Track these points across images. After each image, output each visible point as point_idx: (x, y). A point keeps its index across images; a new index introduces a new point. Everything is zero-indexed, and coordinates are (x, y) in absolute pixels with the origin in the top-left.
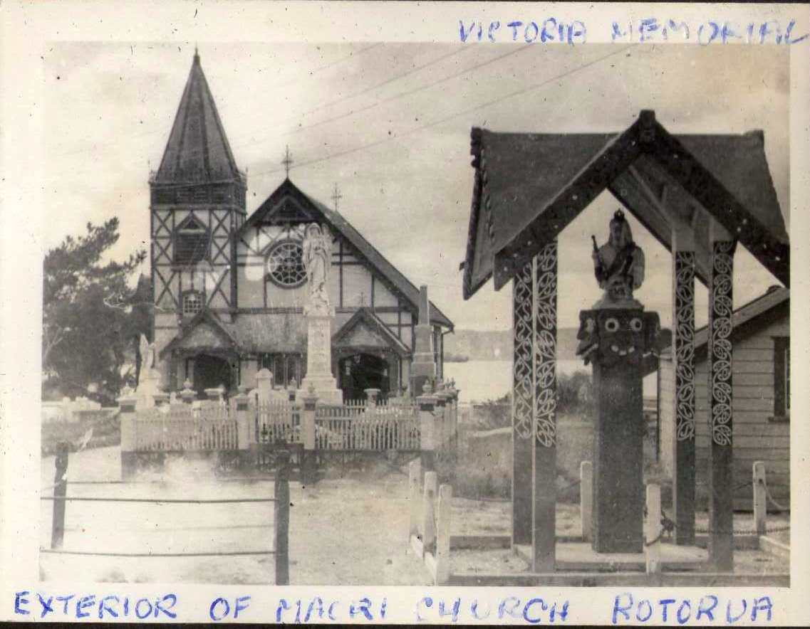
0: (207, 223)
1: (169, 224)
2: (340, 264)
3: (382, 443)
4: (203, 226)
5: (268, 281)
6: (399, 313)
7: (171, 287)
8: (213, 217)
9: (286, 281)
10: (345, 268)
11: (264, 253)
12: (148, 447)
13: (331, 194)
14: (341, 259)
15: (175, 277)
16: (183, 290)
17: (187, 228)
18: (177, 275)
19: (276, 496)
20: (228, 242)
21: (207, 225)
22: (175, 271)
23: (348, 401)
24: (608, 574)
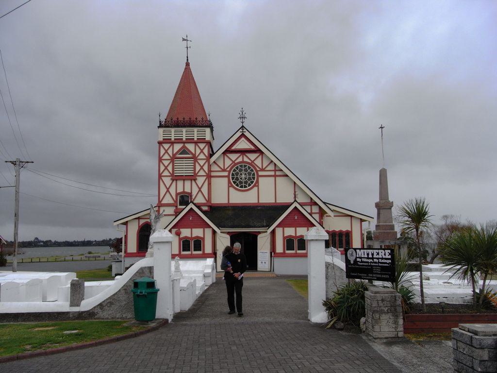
0: (193, 151)
1: (170, 151)
2: (275, 176)
3: (42, 327)
4: (192, 153)
5: (230, 186)
6: (311, 205)
7: (170, 190)
8: (197, 147)
9: (241, 187)
10: (277, 178)
11: (228, 169)
12: (492, 293)
13: (239, 116)
14: (275, 173)
15: (173, 184)
16: (178, 192)
17: (180, 154)
18: (175, 182)
19: (427, 305)
20: (197, 157)
21: (194, 153)
22: (173, 180)
23: (492, 297)
24: (488, 337)
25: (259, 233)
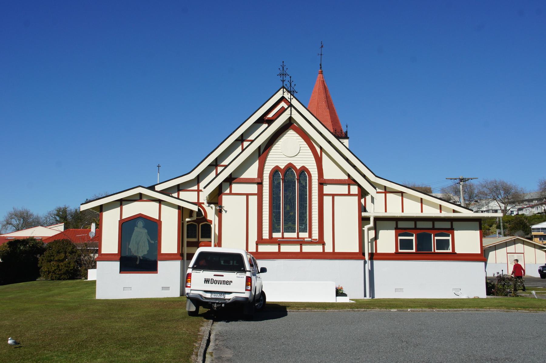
13: (279, 72)
25: (183, 259)
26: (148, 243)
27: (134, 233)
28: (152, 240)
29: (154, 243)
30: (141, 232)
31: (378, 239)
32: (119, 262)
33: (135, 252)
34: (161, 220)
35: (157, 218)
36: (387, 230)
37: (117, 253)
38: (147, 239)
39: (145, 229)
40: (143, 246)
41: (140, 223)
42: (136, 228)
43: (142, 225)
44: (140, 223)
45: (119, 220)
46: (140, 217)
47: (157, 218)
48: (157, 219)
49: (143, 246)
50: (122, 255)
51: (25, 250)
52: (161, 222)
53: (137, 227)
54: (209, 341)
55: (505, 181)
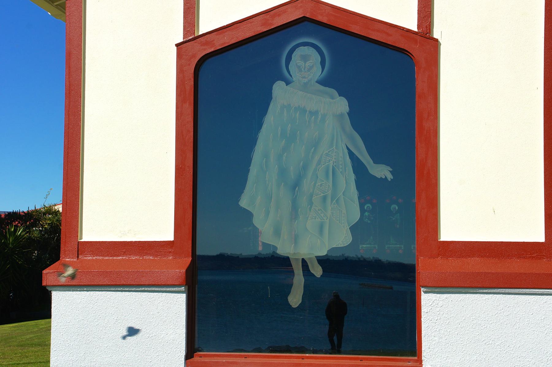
26: (352, 177)
27: (270, 120)
28: (376, 161)
29: (390, 177)
30: (315, 113)
31: (378, 258)
32: (182, 298)
33: (277, 232)
34: (436, 35)
35: (412, 24)
36: (524, 242)
37: (170, 237)
38: (351, 154)
39: (335, 92)
40: (325, 198)
41: (305, 58)
42: (278, 88)
43: (317, 72)
44: (305, 58)
45: (180, 39)
46: (303, 20)
47: (412, 24)
48: (409, 31)
49: (325, 198)
50: (199, 252)
51: (30, 238)
52: (436, 43)
53: (288, 83)
54: (318, 170)
55: (380, 258)
